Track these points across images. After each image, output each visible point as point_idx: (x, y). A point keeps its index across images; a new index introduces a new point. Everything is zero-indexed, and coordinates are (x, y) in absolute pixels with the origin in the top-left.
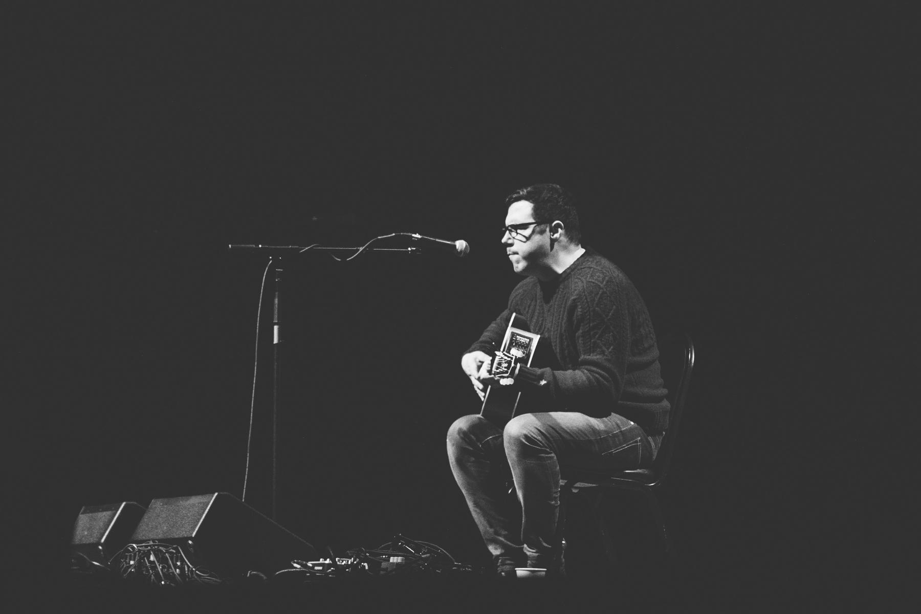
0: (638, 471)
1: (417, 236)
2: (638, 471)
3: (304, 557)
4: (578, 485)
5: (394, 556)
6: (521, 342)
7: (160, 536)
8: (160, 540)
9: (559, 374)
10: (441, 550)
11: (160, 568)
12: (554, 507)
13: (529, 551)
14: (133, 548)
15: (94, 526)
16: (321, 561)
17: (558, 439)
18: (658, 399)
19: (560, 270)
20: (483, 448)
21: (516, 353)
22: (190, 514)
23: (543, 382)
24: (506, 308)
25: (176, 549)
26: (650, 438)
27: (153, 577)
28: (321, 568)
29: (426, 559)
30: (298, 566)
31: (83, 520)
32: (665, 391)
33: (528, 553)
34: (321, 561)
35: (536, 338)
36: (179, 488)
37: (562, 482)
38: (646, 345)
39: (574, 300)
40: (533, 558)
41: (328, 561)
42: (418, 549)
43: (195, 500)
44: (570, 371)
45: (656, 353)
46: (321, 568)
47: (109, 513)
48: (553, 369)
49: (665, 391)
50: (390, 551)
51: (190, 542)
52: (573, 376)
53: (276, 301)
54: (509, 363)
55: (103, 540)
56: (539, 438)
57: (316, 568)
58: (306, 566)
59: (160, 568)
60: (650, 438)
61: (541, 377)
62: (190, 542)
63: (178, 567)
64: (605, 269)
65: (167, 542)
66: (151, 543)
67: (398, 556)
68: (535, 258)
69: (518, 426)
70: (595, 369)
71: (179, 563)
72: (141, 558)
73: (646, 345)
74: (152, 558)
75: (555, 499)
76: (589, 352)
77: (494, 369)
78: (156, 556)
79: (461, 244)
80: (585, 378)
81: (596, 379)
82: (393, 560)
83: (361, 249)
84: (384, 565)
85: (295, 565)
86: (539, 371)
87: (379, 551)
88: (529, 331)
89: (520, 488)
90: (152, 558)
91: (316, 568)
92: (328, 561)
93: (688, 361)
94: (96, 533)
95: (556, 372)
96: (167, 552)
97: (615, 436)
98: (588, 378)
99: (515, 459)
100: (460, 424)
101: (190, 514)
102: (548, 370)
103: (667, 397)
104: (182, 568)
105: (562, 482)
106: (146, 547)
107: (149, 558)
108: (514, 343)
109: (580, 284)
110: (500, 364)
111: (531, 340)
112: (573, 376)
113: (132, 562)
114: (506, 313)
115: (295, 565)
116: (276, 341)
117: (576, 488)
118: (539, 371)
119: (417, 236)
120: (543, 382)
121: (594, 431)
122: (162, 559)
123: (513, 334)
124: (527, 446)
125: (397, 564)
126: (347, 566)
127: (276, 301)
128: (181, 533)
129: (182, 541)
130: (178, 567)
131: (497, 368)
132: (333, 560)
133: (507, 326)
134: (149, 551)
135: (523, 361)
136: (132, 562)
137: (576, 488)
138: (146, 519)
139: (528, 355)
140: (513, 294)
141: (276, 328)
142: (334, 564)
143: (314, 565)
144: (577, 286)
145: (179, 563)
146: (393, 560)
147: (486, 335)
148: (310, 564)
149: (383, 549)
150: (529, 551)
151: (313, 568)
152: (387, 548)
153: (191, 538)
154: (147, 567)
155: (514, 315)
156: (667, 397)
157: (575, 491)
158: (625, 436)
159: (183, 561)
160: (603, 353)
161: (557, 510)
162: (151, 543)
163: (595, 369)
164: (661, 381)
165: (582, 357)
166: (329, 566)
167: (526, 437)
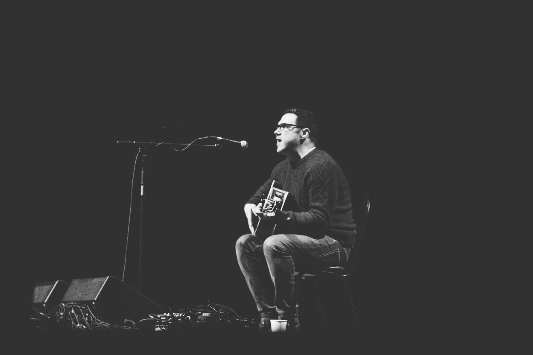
0: (337, 267)
1: (220, 138)
2: (337, 267)
3: (155, 313)
4: (305, 275)
5: (205, 312)
6: (277, 195)
7: (77, 299)
8: (77, 302)
9: (297, 214)
10: (230, 309)
11: (77, 317)
12: (292, 285)
13: (279, 311)
14: (62, 306)
15: (43, 293)
16: (165, 314)
17: (295, 249)
18: (352, 229)
19: (302, 156)
20: (253, 253)
21: (276, 199)
22: (93, 288)
23: (289, 219)
24: (270, 178)
25: (86, 307)
26: (345, 249)
27: (73, 322)
28: (164, 318)
29: (222, 315)
30: (152, 317)
31: (37, 289)
32: (354, 225)
33: (279, 312)
34: (165, 314)
35: (286, 194)
36: (87, 274)
37: (296, 273)
38: (346, 200)
39: (308, 173)
40: (282, 314)
41: (169, 315)
42: (218, 309)
43: (96, 280)
44: (303, 213)
45: (350, 205)
46: (164, 318)
47: (49, 286)
48: (294, 211)
49: (354, 225)
50: (203, 310)
51: (94, 303)
52: (305, 215)
53: (142, 172)
54: (273, 204)
55: (46, 301)
56: (283, 247)
57: (162, 318)
58: (156, 317)
59: (77, 317)
60: (345, 249)
61: (288, 216)
62: (94, 303)
63: (87, 317)
64: (325, 157)
65: (81, 303)
66: (72, 303)
67: (207, 312)
68: (292, 146)
69: (270, 242)
70: (315, 211)
71: (87, 315)
72: (67, 311)
73: (346, 200)
74: (73, 311)
75: (293, 280)
76: (315, 201)
77: (264, 208)
78: (75, 310)
79: (243, 143)
80: (312, 218)
81: (317, 216)
82: (204, 314)
83: (189, 145)
84: (199, 317)
85: (151, 316)
86: (286, 213)
87: (196, 310)
88: (282, 189)
89: (273, 275)
90: (73, 311)
91: (162, 318)
92: (169, 315)
93: (366, 209)
94: (42, 297)
95: (295, 213)
96: (81, 308)
97: (325, 247)
98: (313, 216)
99: (270, 259)
100: (242, 239)
101: (93, 288)
102: (291, 212)
103: (356, 228)
104: (89, 317)
105: (296, 273)
106: (70, 305)
107: (71, 311)
108: (274, 195)
109: (312, 164)
110: (267, 205)
111: (284, 194)
112: (305, 215)
113: (62, 314)
114: (269, 181)
115: (151, 316)
116: (142, 194)
117: (304, 276)
118: (286, 213)
119: (220, 138)
120: (289, 219)
121: (313, 244)
122: (78, 312)
123: (274, 191)
124: (276, 252)
125: (207, 317)
126: (179, 317)
127: (142, 172)
128: (87, 298)
129: (89, 303)
130: (87, 317)
131: (266, 207)
132: (171, 314)
133: (270, 188)
134: (71, 308)
135: (279, 205)
136: (62, 314)
137: (304, 276)
138: (70, 289)
139: (282, 202)
140: (273, 172)
141: (142, 187)
142: (172, 316)
143: (161, 317)
144: (310, 166)
145: (87, 315)
146: (204, 314)
147: (258, 193)
148: (159, 316)
149: (198, 308)
150: (279, 311)
151: (160, 318)
152: (201, 308)
153: (94, 301)
154: (70, 317)
155: (274, 181)
156: (356, 228)
157: (303, 278)
158: (331, 247)
159: (89, 313)
160: (322, 202)
161: (294, 286)
162: (72, 303)
163: (315, 211)
164: (353, 220)
165: (311, 204)
166: (169, 317)
167: (276, 247)
